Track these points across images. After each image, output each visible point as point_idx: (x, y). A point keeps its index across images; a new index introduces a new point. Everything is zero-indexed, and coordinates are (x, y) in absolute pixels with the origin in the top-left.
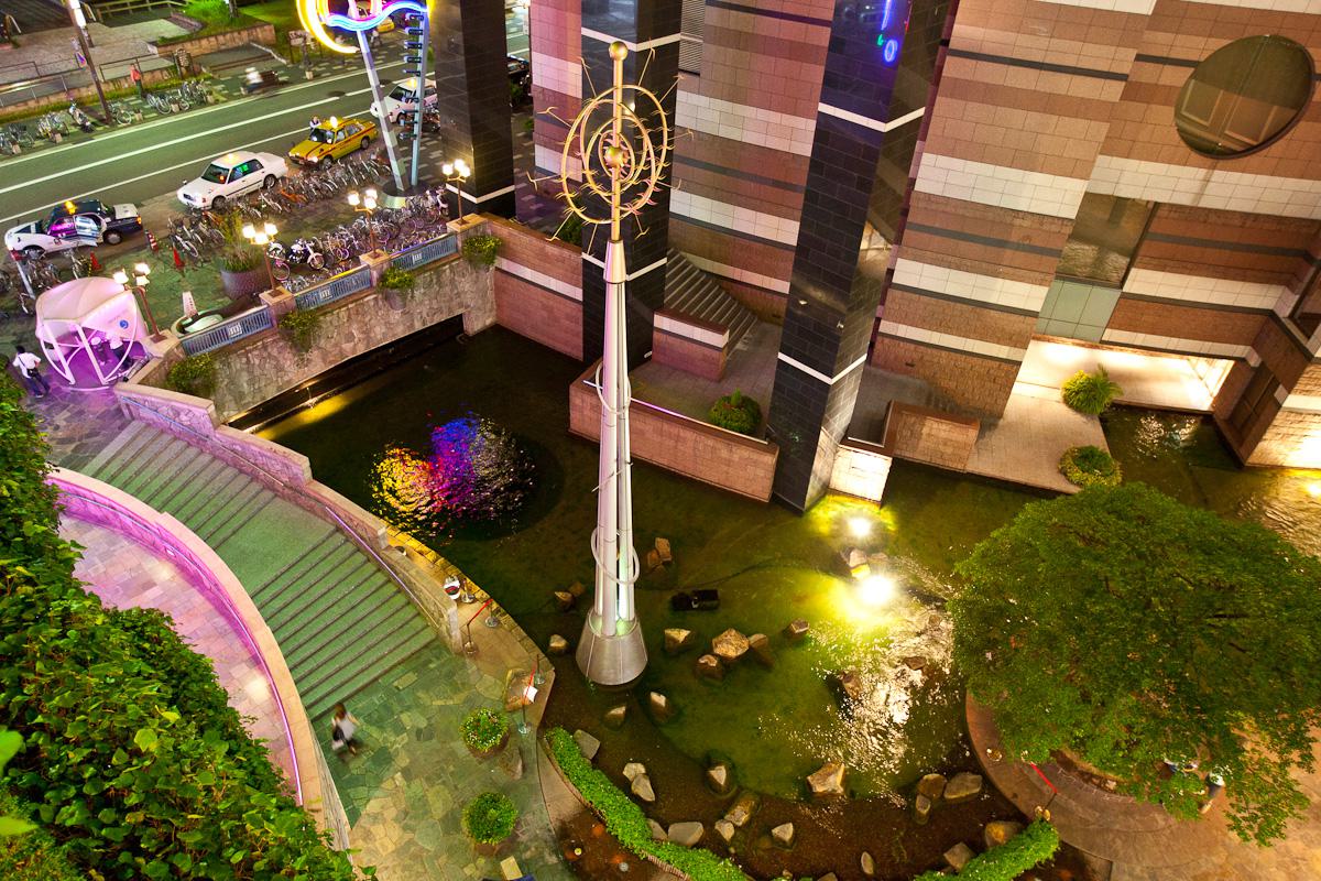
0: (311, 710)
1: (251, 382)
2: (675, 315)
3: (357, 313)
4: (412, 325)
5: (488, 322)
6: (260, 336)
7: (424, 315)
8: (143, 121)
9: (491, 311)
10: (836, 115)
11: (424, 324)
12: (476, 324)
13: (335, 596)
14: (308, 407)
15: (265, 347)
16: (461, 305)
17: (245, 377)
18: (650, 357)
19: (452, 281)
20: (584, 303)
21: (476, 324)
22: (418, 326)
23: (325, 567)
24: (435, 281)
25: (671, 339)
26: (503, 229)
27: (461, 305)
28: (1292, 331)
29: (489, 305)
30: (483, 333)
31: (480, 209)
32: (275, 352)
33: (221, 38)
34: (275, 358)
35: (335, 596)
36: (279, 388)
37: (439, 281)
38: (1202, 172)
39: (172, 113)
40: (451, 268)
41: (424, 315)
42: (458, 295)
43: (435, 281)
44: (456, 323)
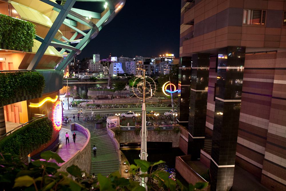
0: (3, 121)
1: (129, 138)
2: (205, 151)
3: (150, 134)
4: (160, 140)
5: (177, 146)
6: (132, 131)
7: (163, 139)
8: (150, 107)
9: (178, 144)
10: (232, 100)
11: (163, 141)
12: (174, 146)
13: (110, 169)
14: (138, 148)
15: (132, 133)
16: (171, 140)
17: (128, 137)
18: (199, 160)
19: (170, 135)
20: (189, 143)
21: (174, 146)
22: (161, 141)
23: (112, 164)
24: (166, 133)
25: (203, 156)
26: (182, 128)
27: (171, 140)
28: (218, 99)
29: (177, 143)
30: (176, 148)
31: (180, 124)
32: (134, 135)
33: (168, 100)
34: (134, 136)
35: (110, 169)
36: (133, 141)
37: (167, 134)
38: (203, 50)
39: (154, 107)
40: (170, 132)
41: (163, 139)
42: (171, 138)
43: (166, 133)
44: (171, 143)
